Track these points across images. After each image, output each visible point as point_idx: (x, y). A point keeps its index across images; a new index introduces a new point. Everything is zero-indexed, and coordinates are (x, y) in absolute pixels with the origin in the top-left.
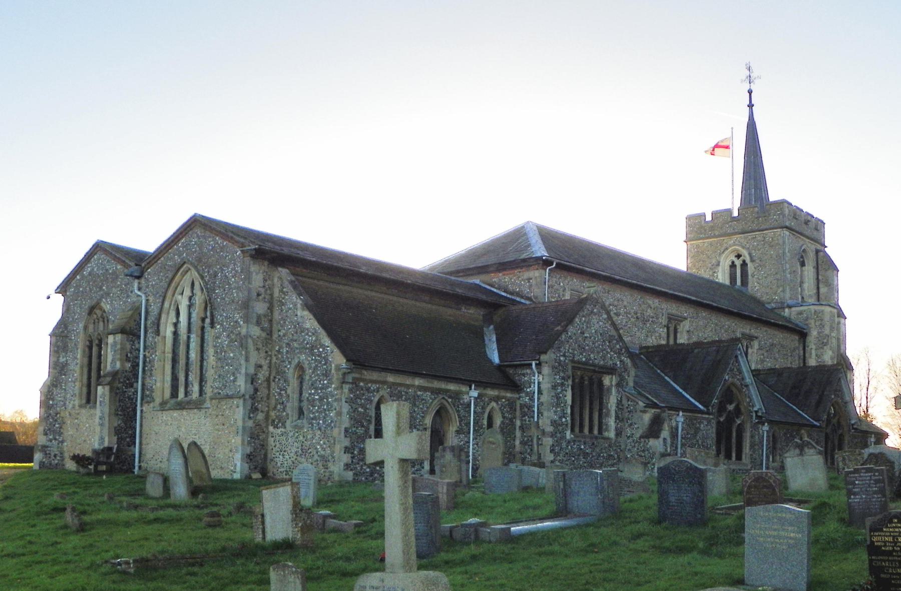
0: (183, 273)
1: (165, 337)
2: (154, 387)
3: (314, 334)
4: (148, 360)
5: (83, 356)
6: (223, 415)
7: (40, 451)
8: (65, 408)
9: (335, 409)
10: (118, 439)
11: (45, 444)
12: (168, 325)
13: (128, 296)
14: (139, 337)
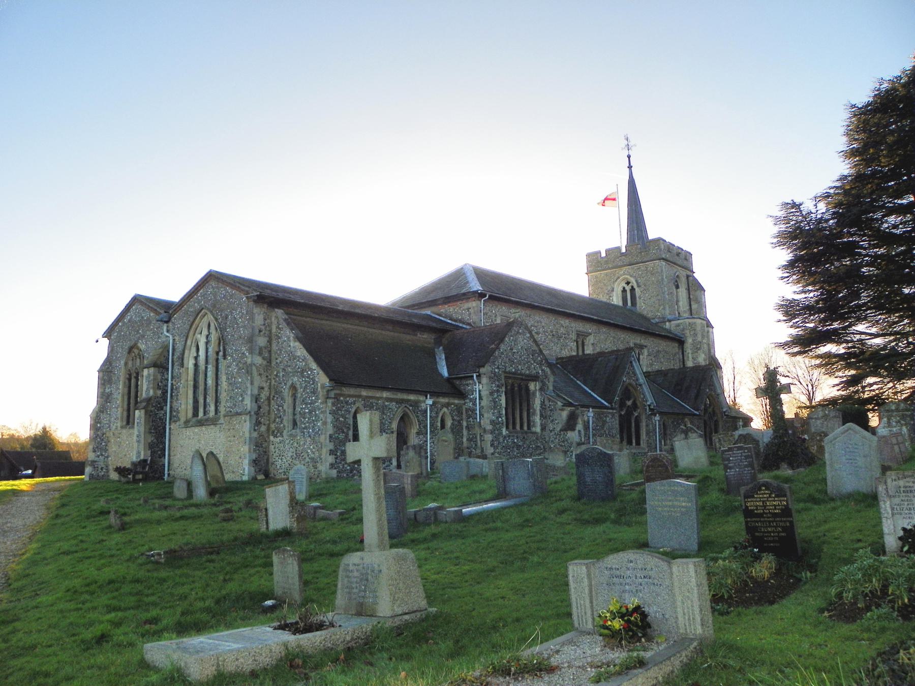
1: (188, 368)
2: (179, 409)
4: (174, 387)
7: (90, 465)
10: (151, 452)
13: (159, 337)
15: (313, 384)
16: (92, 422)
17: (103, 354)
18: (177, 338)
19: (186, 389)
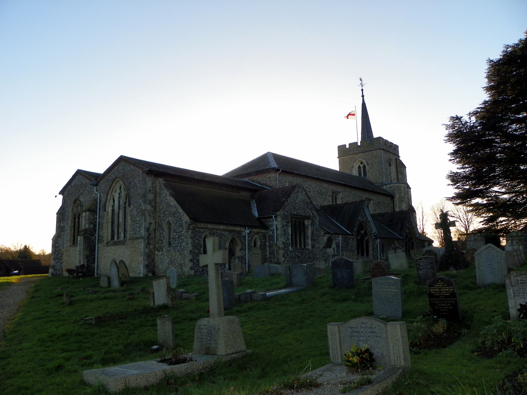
1: (108, 212)
2: (103, 235)
7: (52, 268)
10: (87, 260)
13: (92, 194)
16: (53, 243)
17: (60, 204)
18: (102, 195)
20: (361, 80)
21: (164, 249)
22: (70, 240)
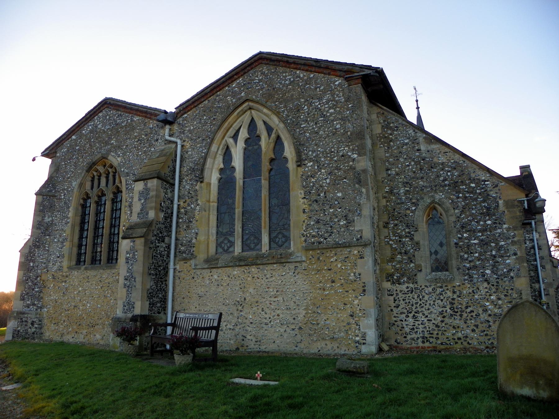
0: (241, 113)
1: (210, 184)
2: (194, 241)
3: (455, 169)
4: (182, 210)
5: (76, 215)
6: (330, 270)
7: (15, 318)
8: (48, 271)
9: (515, 254)
10: (150, 304)
11: (21, 310)
12: (214, 170)
13: (151, 146)
14: (173, 185)
15: (484, 201)
16: (23, 260)
17: (43, 177)
18: (187, 145)
19: (207, 212)
20: (415, 89)
21: (420, 277)
22: (70, 254)
